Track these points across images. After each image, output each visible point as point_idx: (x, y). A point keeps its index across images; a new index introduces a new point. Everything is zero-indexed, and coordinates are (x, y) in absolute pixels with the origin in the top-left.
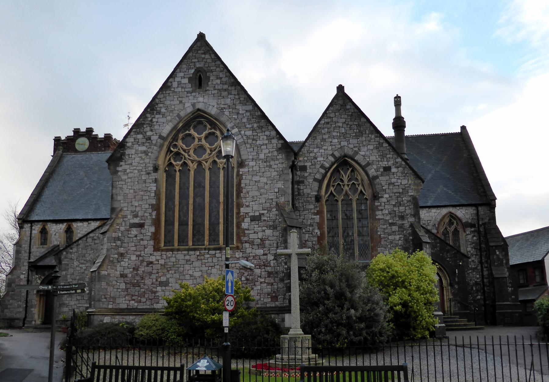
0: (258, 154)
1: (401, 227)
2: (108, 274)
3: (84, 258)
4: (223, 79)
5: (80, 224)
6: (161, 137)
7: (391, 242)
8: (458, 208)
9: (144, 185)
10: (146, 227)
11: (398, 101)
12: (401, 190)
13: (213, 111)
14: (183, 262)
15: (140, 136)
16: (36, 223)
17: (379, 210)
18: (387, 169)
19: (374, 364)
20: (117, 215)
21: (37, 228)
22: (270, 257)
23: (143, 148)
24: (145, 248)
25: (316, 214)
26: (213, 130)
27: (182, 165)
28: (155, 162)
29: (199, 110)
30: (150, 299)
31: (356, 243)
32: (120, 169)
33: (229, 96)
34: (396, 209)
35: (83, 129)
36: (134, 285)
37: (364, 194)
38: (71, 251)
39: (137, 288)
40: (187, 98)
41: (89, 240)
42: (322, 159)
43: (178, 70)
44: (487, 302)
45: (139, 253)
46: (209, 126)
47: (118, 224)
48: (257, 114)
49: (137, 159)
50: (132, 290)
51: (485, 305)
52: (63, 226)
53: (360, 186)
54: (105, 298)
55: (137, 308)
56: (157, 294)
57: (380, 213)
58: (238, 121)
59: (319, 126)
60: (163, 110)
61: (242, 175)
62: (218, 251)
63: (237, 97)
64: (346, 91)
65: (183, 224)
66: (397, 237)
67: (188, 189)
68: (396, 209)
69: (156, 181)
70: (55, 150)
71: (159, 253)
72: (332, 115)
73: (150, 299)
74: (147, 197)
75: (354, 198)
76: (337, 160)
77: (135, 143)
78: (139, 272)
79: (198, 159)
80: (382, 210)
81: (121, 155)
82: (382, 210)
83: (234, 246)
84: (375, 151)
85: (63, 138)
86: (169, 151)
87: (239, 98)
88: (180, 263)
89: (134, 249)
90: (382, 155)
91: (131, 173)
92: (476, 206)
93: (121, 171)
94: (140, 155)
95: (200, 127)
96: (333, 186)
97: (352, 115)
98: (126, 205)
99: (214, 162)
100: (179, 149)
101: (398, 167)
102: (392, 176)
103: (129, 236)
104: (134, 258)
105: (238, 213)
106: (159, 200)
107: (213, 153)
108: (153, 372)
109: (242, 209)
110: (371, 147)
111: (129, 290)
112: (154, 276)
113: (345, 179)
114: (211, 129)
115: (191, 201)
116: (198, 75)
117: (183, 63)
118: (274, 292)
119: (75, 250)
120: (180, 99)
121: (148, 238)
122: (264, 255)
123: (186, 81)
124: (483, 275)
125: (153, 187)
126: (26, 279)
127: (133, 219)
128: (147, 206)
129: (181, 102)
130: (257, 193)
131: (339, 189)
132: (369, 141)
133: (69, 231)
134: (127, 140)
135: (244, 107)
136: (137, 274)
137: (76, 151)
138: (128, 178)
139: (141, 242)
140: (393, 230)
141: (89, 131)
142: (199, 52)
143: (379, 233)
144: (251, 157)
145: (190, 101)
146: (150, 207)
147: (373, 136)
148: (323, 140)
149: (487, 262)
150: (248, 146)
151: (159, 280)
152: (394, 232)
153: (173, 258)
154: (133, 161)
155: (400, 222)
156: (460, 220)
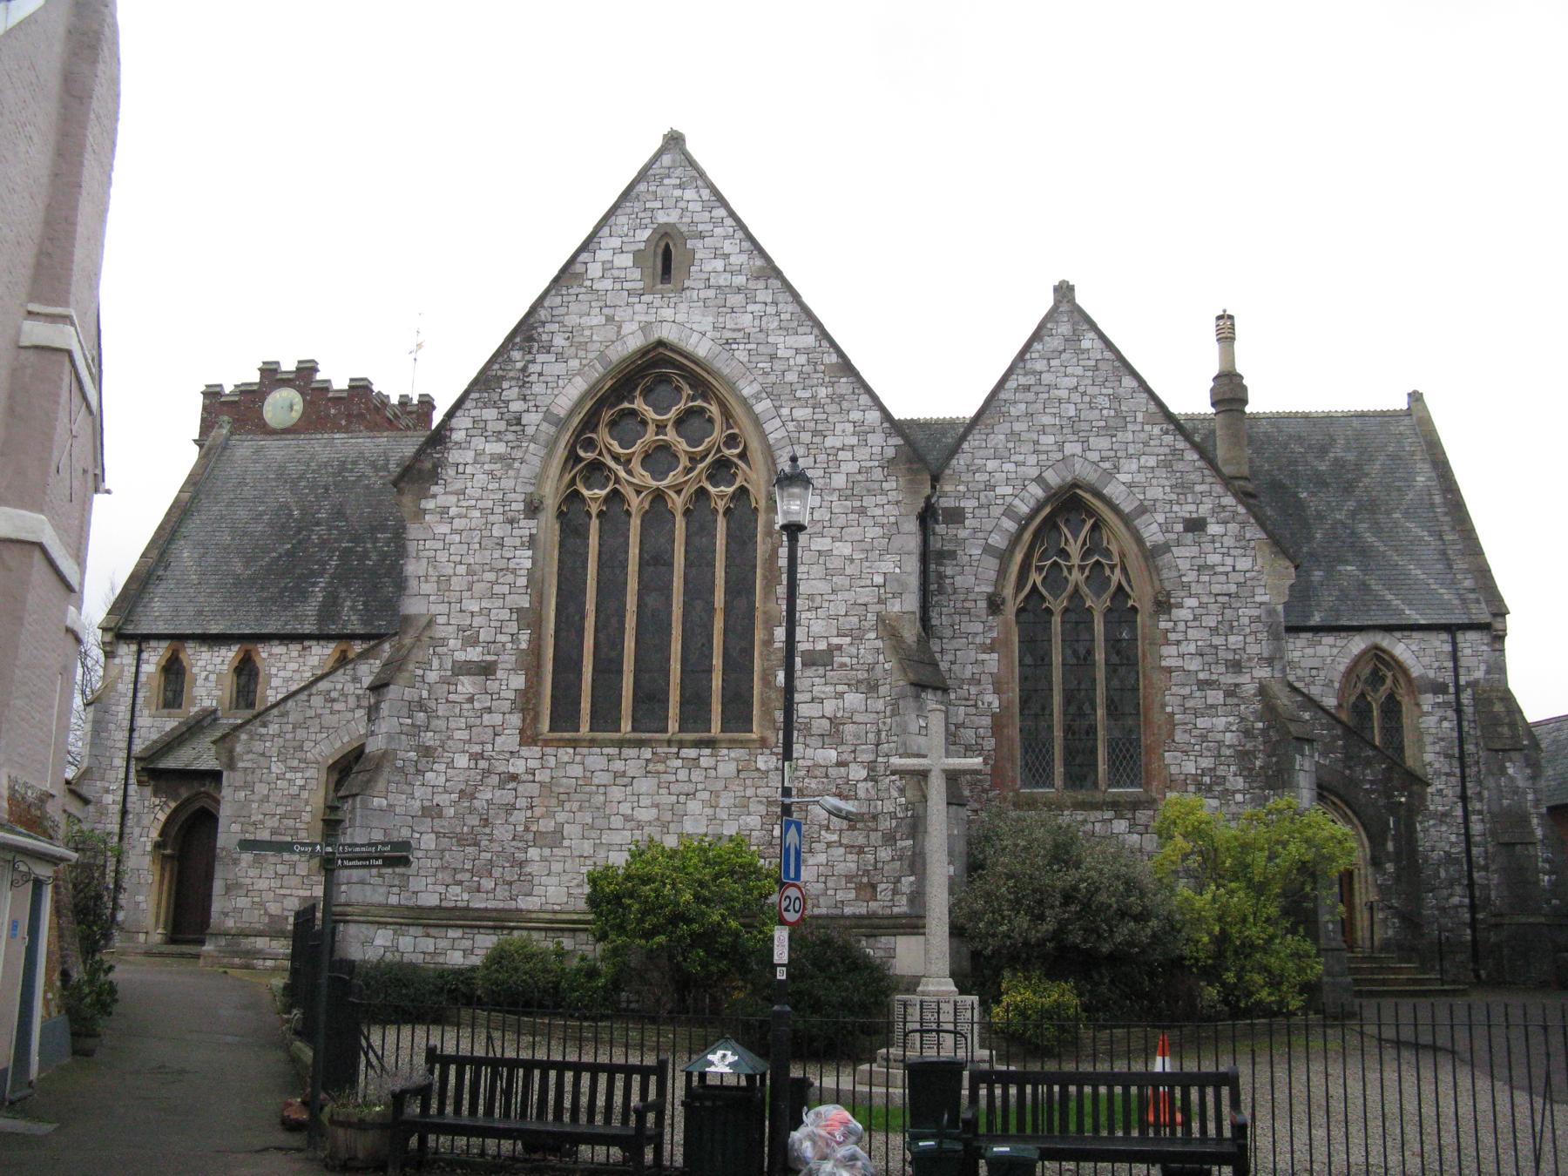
2: (389, 805)
3: (299, 755)
4: (732, 259)
5: (278, 649)
6: (548, 416)
7: (1203, 738)
8: (1398, 635)
9: (497, 554)
10: (500, 674)
11: (1226, 330)
12: (1233, 588)
13: (701, 348)
15: (490, 414)
16: (153, 644)
18: (1195, 525)
20: (418, 639)
22: (858, 773)
23: (500, 448)
25: (991, 649)
27: (607, 499)
28: (530, 489)
29: (661, 343)
32: (429, 504)
33: (750, 308)
34: (1217, 641)
36: (461, 841)
37: (1129, 596)
38: (263, 731)
39: (469, 849)
40: (630, 311)
41: (317, 701)
42: (1009, 490)
43: (606, 230)
44: (1480, 916)
45: (477, 749)
46: (687, 390)
49: (481, 478)
50: (455, 856)
51: (1473, 924)
52: (228, 656)
53: (1117, 571)
55: (467, 909)
56: (528, 870)
57: (1173, 650)
58: (772, 378)
59: (1002, 396)
60: (559, 341)
62: (707, 751)
63: (771, 310)
64: (1081, 299)
65: (608, 668)
66: (1221, 722)
68: (1217, 641)
69: (532, 542)
72: (1040, 365)
74: (506, 589)
75: (1098, 605)
79: (655, 484)
80: (1178, 643)
81: (435, 467)
82: (1178, 643)
84: (1162, 473)
85: (228, 389)
86: (573, 458)
87: (778, 314)
88: (596, 781)
89: (464, 735)
91: (460, 516)
93: (432, 512)
95: (663, 390)
96: (1040, 569)
97: (1096, 368)
98: (443, 608)
99: (702, 492)
100: (600, 454)
101: (1226, 523)
102: (1208, 547)
104: (462, 761)
110: (1152, 462)
111: (447, 854)
112: (519, 817)
113: (1074, 549)
114: (693, 399)
116: (662, 244)
117: (619, 211)
119: (273, 728)
120: (605, 311)
122: (840, 764)
123: (626, 260)
124: (1468, 836)
125: (524, 559)
126: (118, 807)
127: (463, 649)
128: (505, 614)
129: (610, 319)
130: (823, 587)
131: (1055, 577)
132: (1146, 444)
133: (246, 671)
134: (454, 423)
135: (792, 341)
136: (472, 810)
137: (265, 430)
138: (453, 531)
139: (486, 716)
140: (1209, 701)
141: (307, 370)
142: (666, 181)
143: (1169, 709)
145: (637, 318)
146: (515, 616)
147: (1156, 430)
148: (1013, 435)
151: (534, 828)
152: (1212, 706)
153: (569, 764)
154: (469, 484)
155: (1230, 679)
156: (1405, 671)
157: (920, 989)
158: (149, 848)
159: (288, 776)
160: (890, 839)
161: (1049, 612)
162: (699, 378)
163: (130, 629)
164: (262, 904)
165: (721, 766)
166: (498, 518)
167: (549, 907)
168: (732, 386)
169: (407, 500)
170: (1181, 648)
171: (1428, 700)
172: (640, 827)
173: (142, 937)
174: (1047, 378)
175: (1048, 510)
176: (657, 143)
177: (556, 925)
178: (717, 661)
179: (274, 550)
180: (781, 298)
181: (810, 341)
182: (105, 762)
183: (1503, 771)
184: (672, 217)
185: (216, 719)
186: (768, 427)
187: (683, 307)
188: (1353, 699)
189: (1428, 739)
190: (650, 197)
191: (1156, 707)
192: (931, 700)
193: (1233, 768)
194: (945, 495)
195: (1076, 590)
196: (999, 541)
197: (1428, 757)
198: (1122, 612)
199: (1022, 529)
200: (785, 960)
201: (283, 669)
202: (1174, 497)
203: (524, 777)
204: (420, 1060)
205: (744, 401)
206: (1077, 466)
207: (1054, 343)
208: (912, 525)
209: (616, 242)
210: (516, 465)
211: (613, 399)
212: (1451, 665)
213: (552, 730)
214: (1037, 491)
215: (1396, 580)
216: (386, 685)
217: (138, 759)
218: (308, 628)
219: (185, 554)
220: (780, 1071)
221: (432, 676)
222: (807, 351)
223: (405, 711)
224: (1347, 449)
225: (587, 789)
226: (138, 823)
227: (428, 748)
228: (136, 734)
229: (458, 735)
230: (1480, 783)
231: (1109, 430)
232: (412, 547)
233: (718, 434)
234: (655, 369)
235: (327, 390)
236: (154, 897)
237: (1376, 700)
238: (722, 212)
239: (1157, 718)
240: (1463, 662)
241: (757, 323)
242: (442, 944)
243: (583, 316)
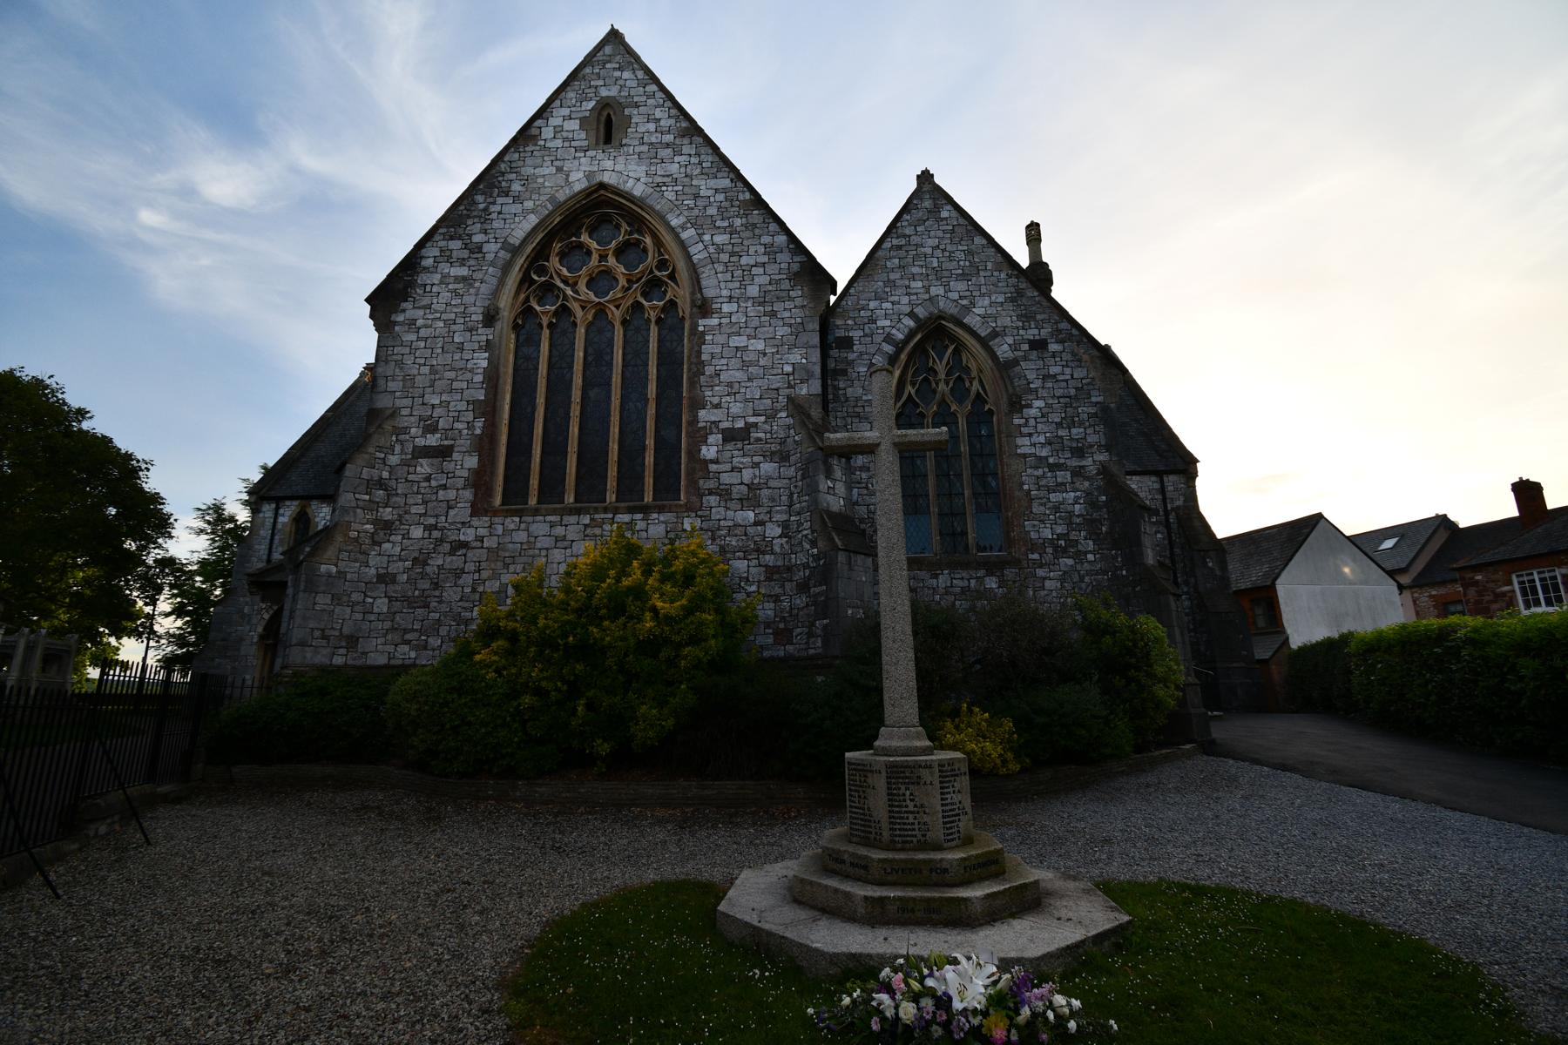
0: (743, 286)
1: (1078, 473)
6: (506, 246)
7: (1056, 509)
9: (457, 356)
10: (455, 456)
12: (1073, 392)
15: (455, 245)
17: (1022, 435)
18: (1039, 345)
22: (773, 531)
23: (463, 271)
24: (449, 508)
27: (556, 313)
29: (602, 186)
32: (400, 318)
33: (677, 159)
36: (410, 602)
40: (576, 162)
42: (888, 323)
43: (558, 102)
45: (432, 521)
46: (625, 227)
47: (380, 448)
48: (741, 197)
53: (976, 384)
54: (324, 637)
57: (1026, 441)
58: (696, 212)
60: (516, 187)
61: (703, 333)
62: (639, 516)
67: (571, 367)
69: (488, 347)
76: (921, 324)
78: (428, 569)
80: (1030, 435)
81: (406, 288)
82: (1030, 435)
84: (1010, 306)
86: (526, 280)
87: (700, 163)
88: (539, 545)
90: (1025, 316)
91: (426, 326)
92: (1159, 474)
95: (605, 232)
97: (953, 232)
98: (408, 402)
99: (637, 306)
101: (1062, 342)
103: (411, 477)
104: (417, 532)
109: (702, 413)
112: (467, 579)
113: (941, 368)
115: (576, 395)
118: (783, 619)
120: (557, 163)
122: (756, 524)
127: (423, 436)
128: (462, 406)
129: (560, 169)
131: (926, 389)
134: (424, 252)
136: (423, 575)
139: (441, 492)
144: (725, 293)
148: (892, 284)
149: (1186, 583)
150: (721, 268)
151: (481, 589)
155: (1075, 463)
157: (877, 743)
160: (803, 587)
165: (651, 528)
168: (662, 218)
178: (650, 442)
181: (726, 183)
184: (613, 92)
186: (692, 250)
187: (621, 159)
198: (980, 416)
205: (672, 230)
209: (566, 112)
221: (394, 460)
222: (724, 191)
223: (363, 488)
231: (965, 277)
233: (651, 259)
234: (599, 208)
238: (654, 88)
240: (1169, 495)
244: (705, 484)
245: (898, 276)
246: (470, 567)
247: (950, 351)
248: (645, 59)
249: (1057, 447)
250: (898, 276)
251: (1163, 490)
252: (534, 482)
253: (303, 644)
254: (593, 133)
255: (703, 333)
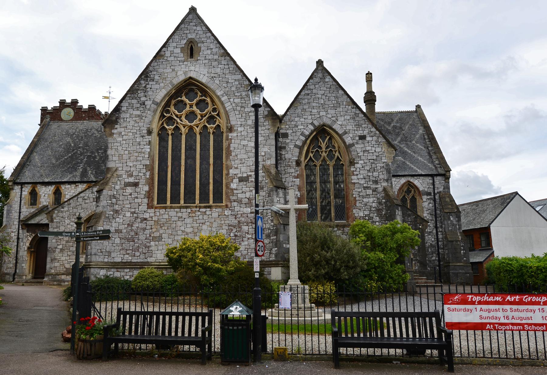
4: (213, 50)
5: (68, 186)
6: (154, 102)
7: (366, 205)
8: (416, 178)
9: (138, 147)
10: (140, 186)
11: (369, 77)
12: (375, 158)
14: (176, 219)
15: (134, 101)
16: (26, 185)
18: (363, 138)
19: (369, 310)
20: (112, 175)
21: (27, 190)
23: (138, 113)
25: (297, 177)
26: (203, 98)
27: (174, 129)
28: (149, 126)
29: (190, 78)
30: (143, 253)
31: (333, 204)
32: (114, 131)
33: (220, 66)
34: (370, 174)
35: (69, 101)
36: (128, 240)
37: (341, 161)
38: (62, 210)
40: (180, 67)
41: (80, 200)
42: (302, 127)
43: (171, 40)
44: (442, 263)
45: (133, 210)
46: (199, 94)
48: (245, 83)
49: (132, 123)
50: (126, 245)
51: (439, 265)
52: (52, 188)
53: (337, 152)
54: (101, 252)
55: (131, 262)
57: (355, 177)
58: (227, 89)
59: (300, 97)
60: (157, 77)
61: (231, 139)
63: (226, 67)
64: (325, 65)
65: (176, 183)
66: (371, 200)
68: (370, 174)
70: (42, 119)
71: (153, 210)
72: (312, 87)
73: (143, 253)
74: (141, 158)
75: (331, 163)
77: (129, 107)
79: (190, 124)
80: (357, 175)
81: (117, 119)
82: (357, 175)
83: (223, 204)
84: (352, 121)
85: (49, 108)
86: (162, 116)
87: (229, 68)
88: (172, 220)
89: (129, 206)
93: (116, 134)
94: (134, 119)
95: (191, 94)
96: (312, 152)
98: (121, 165)
99: (205, 127)
100: (172, 114)
101: (372, 137)
102: (367, 145)
103: (124, 194)
104: (128, 214)
105: (228, 174)
106: (153, 161)
107: (204, 118)
108: (161, 317)
109: (231, 171)
110: (348, 117)
112: (147, 232)
113: (323, 146)
114: (201, 96)
116: (190, 45)
117: (175, 34)
120: (172, 67)
121: (143, 196)
123: (178, 50)
124: (437, 238)
125: (147, 149)
126: (16, 237)
128: (141, 167)
129: (173, 70)
130: (245, 156)
131: (317, 155)
132: (346, 112)
133: (58, 194)
134: (122, 104)
136: (132, 230)
137: (61, 120)
138: (123, 140)
139: (136, 200)
140: (367, 193)
141: (75, 102)
142: (191, 24)
143: (354, 196)
144: (239, 123)
145: (182, 70)
146: (145, 167)
147: (350, 107)
148: (304, 110)
149: (441, 227)
150: (237, 113)
151: (152, 235)
152: (368, 195)
153: (164, 214)
155: (374, 186)
158: (26, 249)
159: (71, 224)
160: (268, 236)
161: (315, 166)
162: (203, 90)
163: (18, 181)
164: (63, 265)
166: (138, 135)
167: (158, 261)
168: (214, 92)
169: (107, 130)
170: (358, 176)
171: (425, 198)
172: (187, 234)
173: (24, 277)
174: (314, 91)
175: (315, 133)
176: (188, 11)
177: (159, 267)
178: (211, 181)
179: (66, 156)
180: (230, 63)
182: (12, 223)
183: (449, 219)
185: (48, 209)
186: (226, 105)
187: (197, 66)
188: (401, 197)
189: (425, 209)
190: (185, 29)
191: (350, 195)
192: (281, 192)
193: (375, 214)
194: (282, 129)
195: (324, 159)
196: (299, 143)
197: (425, 215)
198: (339, 166)
199: (307, 139)
200: (258, 270)
201: (68, 191)
202: (356, 129)
203: (149, 219)
204: (115, 312)
205: (218, 97)
206: (324, 120)
207: (316, 80)
208: (273, 137)
209: (175, 44)
210: (144, 118)
211: (175, 97)
212: (432, 187)
213: (157, 204)
214: (312, 128)
215: (415, 162)
216: (102, 190)
217: (22, 221)
218: (77, 179)
219: (36, 158)
220: (257, 313)
221: (117, 187)
222: (239, 80)
223: (109, 198)
224: (397, 122)
225: (170, 222)
226: (22, 241)
227: (117, 210)
228: (21, 214)
229: (126, 206)
230: (441, 223)
231: (335, 108)
232: (110, 145)
233: (210, 108)
234: (190, 86)
235: (81, 109)
236: (28, 264)
237: (409, 198)
238: (210, 34)
239: (351, 199)
240: (436, 186)
241: (222, 71)
242: (122, 274)
243: (165, 69)
244: (233, 198)
245: (307, 107)
246: (148, 227)
247: (327, 139)
248: (205, 21)
249: (367, 180)
250: (307, 107)
251: (433, 184)
252: (169, 196)
253: (95, 254)
254: (186, 54)
255: (231, 139)
